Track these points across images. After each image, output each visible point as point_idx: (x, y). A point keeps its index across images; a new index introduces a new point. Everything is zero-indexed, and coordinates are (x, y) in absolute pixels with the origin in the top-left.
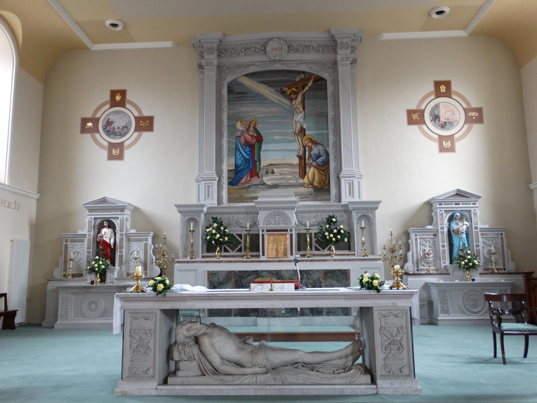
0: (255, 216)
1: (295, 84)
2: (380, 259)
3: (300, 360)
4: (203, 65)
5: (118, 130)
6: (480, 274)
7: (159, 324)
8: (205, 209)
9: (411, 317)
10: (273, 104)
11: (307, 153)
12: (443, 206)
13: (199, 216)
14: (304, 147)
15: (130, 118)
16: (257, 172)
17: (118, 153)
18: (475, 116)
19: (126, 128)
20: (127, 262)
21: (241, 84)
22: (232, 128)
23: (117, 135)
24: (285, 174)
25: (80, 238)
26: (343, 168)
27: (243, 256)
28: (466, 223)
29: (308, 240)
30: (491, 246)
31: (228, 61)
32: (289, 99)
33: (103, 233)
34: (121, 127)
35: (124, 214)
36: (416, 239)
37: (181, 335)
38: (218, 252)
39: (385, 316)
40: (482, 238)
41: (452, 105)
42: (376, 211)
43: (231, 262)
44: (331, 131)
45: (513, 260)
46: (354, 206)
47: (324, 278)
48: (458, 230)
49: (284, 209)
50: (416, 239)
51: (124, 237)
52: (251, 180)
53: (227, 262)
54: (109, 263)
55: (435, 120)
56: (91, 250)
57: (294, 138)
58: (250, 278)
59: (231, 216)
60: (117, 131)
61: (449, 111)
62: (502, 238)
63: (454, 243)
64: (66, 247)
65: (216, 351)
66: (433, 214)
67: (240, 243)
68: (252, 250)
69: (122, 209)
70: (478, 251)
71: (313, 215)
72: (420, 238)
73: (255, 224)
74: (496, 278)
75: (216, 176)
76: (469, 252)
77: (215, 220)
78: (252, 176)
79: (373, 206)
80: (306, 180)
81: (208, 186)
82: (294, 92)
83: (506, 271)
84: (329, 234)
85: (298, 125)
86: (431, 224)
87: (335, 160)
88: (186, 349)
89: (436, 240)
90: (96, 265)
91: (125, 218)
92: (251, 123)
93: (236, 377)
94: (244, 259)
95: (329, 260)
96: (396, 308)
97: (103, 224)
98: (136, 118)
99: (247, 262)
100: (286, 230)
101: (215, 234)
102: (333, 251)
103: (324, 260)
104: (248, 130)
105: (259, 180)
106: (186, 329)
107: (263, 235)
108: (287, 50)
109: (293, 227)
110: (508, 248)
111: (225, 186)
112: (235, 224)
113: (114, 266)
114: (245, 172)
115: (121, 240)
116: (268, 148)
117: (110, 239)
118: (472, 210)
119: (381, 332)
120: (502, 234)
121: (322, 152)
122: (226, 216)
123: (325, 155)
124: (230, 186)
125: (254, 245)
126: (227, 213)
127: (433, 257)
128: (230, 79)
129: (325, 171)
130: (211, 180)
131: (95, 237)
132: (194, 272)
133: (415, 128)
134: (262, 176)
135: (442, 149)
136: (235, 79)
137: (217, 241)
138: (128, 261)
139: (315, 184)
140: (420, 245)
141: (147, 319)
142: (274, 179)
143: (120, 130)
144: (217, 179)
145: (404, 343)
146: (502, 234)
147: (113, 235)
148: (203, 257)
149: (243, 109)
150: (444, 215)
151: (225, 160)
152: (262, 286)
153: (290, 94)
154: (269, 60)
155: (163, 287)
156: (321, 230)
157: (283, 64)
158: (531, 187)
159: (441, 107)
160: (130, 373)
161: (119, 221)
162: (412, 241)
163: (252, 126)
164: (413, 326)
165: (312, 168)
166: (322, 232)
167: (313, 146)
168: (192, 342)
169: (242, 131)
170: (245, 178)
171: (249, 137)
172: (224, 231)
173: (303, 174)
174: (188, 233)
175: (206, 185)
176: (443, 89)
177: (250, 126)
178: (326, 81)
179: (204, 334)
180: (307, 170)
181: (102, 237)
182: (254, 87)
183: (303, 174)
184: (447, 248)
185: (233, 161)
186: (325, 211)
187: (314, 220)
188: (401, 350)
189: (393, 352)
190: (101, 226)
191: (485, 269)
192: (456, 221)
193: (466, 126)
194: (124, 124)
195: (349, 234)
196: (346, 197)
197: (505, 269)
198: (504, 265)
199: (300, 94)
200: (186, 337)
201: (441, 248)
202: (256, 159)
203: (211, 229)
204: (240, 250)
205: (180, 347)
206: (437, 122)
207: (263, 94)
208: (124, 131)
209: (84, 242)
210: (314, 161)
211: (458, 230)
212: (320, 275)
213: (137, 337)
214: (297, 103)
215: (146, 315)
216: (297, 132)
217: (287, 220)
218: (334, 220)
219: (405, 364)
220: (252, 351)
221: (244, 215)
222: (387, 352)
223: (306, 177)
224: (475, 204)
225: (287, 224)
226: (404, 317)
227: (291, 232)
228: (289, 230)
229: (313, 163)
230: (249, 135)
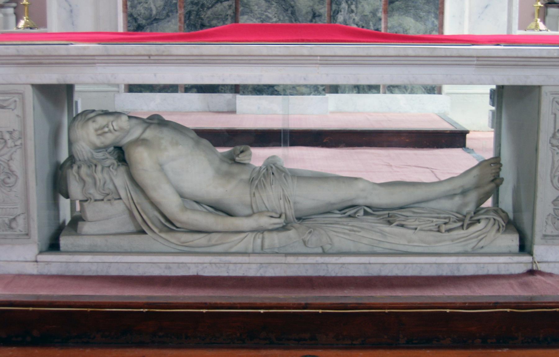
3: (360, 201)
65: (169, 181)
88: (99, 176)
93: (215, 237)
106: (96, 130)
168: (111, 160)
179: (140, 141)
200: (98, 149)
205: (84, 170)
220: (251, 181)
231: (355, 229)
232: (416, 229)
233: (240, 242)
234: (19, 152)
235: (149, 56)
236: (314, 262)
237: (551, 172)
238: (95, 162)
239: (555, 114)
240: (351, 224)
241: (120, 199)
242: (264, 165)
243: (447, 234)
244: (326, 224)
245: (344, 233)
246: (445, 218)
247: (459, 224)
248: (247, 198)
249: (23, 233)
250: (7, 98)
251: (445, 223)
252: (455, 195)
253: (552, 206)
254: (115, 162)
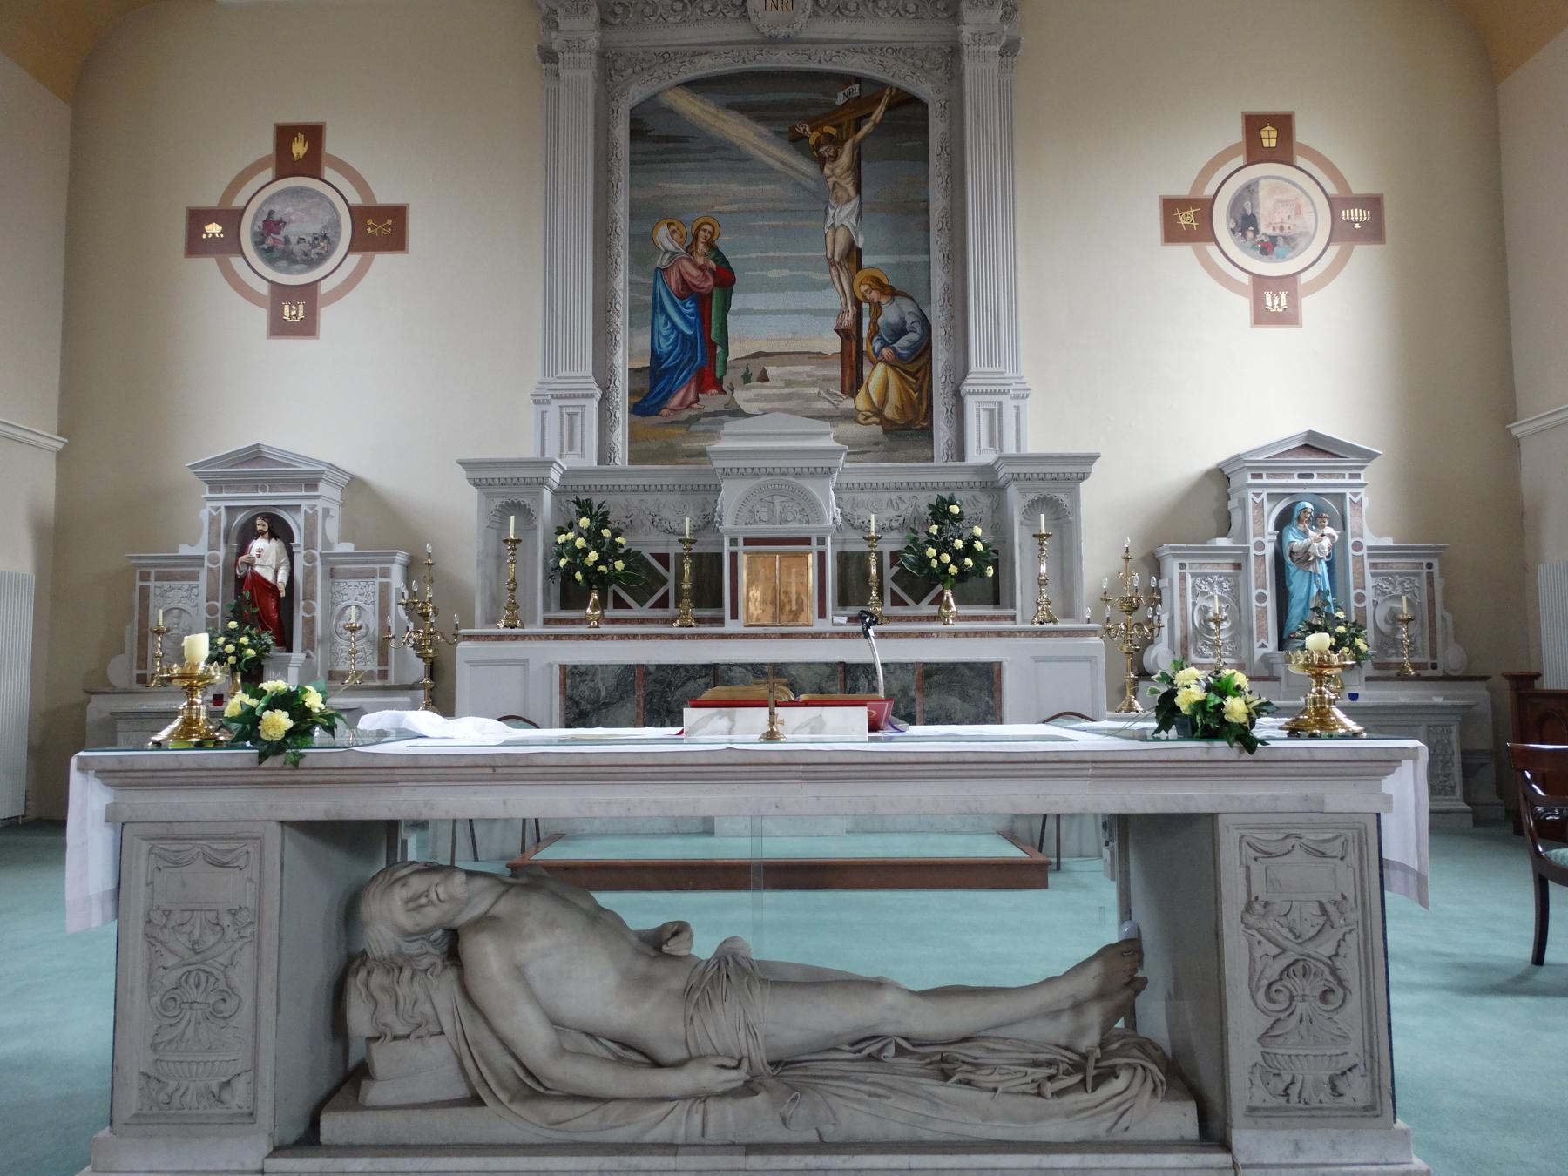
0: (710, 497)
2: (1093, 632)
3: (888, 1029)
4: (555, 48)
5: (302, 246)
6: (1368, 679)
8: (555, 476)
9: (1381, 859)
11: (866, 321)
12: (1265, 481)
13: (538, 497)
14: (858, 304)
15: (336, 211)
16: (718, 375)
17: (301, 316)
19: (323, 242)
20: (329, 639)
21: (670, 111)
22: (642, 245)
23: (296, 262)
24: (799, 383)
26: (973, 367)
27: (673, 620)
28: (1328, 530)
29: (874, 571)
30: (1399, 598)
32: (813, 159)
33: (254, 553)
34: (309, 239)
35: (317, 497)
36: (1183, 578)
37: (382, 928)
38: (595, 607)
39: (1269, 855)
40: (1374, 575)
41: (1295, 185)
42: (1083, 485)
43: (634, 637)
44: (937, 255)
45: (1457, 639)
46: (1016, 470)
47: (920, 689)
48: (1306, 551)
49: (798, 474)
50: (1183, 578)
51: (318, 563)
52: (697, 400)
53: (622, 637)
54: (270, 641)
55: (1243, 231)
56: (219, 605)
57: (827, 277)
58: (691, 686)
59: (634, 498)
60: (296, 248)
61: (1285, 203)
62: (1430, 577)
63: (1291, 588)
64: (144, 592)
65: (534, 998)
66: (1232, 504)
67: (664, 581)
68: (698, 604)
69: (310, 481)
70: (1361, 612)
71: (886, 496)
72: (1193, 575)
73: (708, 523)
74: (1418, 692)
75: (595, 386)
76: (1341, 615)
77: (585, 508)
78: (701, 389)
79: (1076, 468)
80: (861, 402)
81: (571, 415)
82: (830, 139)
83: (1438, 673)
84: (939, 554)
85: (841, 237)
86: (1224, 533)
87: (947, 342)
88: (403, 990)
89: (1241, 580)
90: (230, 648)
91: (319, 509)
92: (699, 228)
93: (615, 1110)
94: (675, 629)
95: (938, 634)
96: (1316, 818)
97: (255, 525)
98: (352, 210)
99: (682, 637)
100: (807, 541)
101: (585, 552)
102: (948, 606)
103: (922, 634)
104: (691, 249)
105: (724, 399)
106: (407, 902)
107: (734, 556)
108: (809, 6)
109: (828, 530)
110: (1446, 606)
111: (622, 415)
112: (649, 524)
113: (290, 650)
114: (682, 374)
115: (309, 574)
116: (748, 306)
117: (276, 572)
118: (1348, 492)
119: (1251, 920)
120: (1430, 566)
121: (909, 320)
122: (620, 498)
123: (918, 327)
124: (637, 418)
125: (707, 589)
126: (623, 490)
127: (1230, 628)
128: (637, 92)
129: (920, 375)
130: (578, 397)
131: (230, 567)
132: (517, 670)
133: (1185, 251)
134: (732, 390)
135: (1262, 317)
136: (654, 96)
137: (590, 572)
138: (331, 636)
139: (889, 412)
140: (1192, 593)
141: (223, 865)
142: (766, 398)
143: (305, 247)
144: (598, 394)
145: (1350, 968)
146: (1430, 566)
147: (285, 559)
148: (547, 622)
149: (677, 187)
150: (1267, 507)
151: (622, 337)
152: (732, 720)
153: (818, 145)
154: (757, 37)
155: (289, 724)
156: (914, 541)
157: (797, 52)
158: (1515, 432)
159: (1262, 193)
160: (147, 1095)
161: (301, 519)
162: (1171, 581)
164: (1387, 894)
165: (881, 366)
166: (915, 547)
167: (883, 300)
168: (432, 956)
169: (673, 254)
170: (681, 394)
171: (695, 272)
172: (612, 542)
173: (853, 383)
175: (565, 411)
176: (1269, 138)
177: (696, 238)
178: (925, 106)
179: (485, 922)
180: (866, 371)
181: (251, 564)
182: (708, 118)
183: (853, 383)
184: (1270, 604)
185: (644, 342)
186: (923, 487)
187: (892, 513)
188: (1335, 1000)
189: (1301, 1007)
190: (247, 534)
191: (1377, 666)
192: (1301, 527)
193: (1334, 250)
194: (316, 228)
195: (998, 555)
196: (980, 451)
197: (1434, 667)
198: (1434, 656)
199: (848, 146)
200: (409, 936)
201: (1254, 603)
202: (713, 337)
203: (571, 535)
204: (663, 603)
205: (378, 978)
206: (1250, 235)
207: (739, 142)
208: (317, 250)
209: (197, 579)
210: (885, 345)
211: (1306, 551)
212: (911, 679)
213: (180, 943)
214: (838, 171)
215: (222, 849)
216: (837, 259)
217: (810, 509)
218: (955, 509)
219: (1351, 1060)
220: (688, 992)
221: (677, 497)
222: (1277, 1007)
223: (862, 392)
224: (1358, 476)
225: (808, 522)
226: (1352, 858)
227: (821, 548)
228: (814, 541)
229: (885, 351)
230: (695, 264)
231: (880, 1091)
232: (995, 1090)
233: (658, 1123)
234: (248, 950)
235: (494, 767)
236: (801, 1166)
237: (1251, 979)
238: (400, 961)
239: (1248, 868)
240: (872, 1078)
241: (442, 1033)
242: (715, 956)
243: (1055, 1101)
244: (826, 1077)
245: (859, 1101)
246: (1050, 1064)
247: (1077, 1078)
248: (680, 1029)
249: (245, 1110)
250: (233, 846)
251: (1051, 1078)
252: (1061, 1011)
253: (1259, 1049)
254: (439, 962)
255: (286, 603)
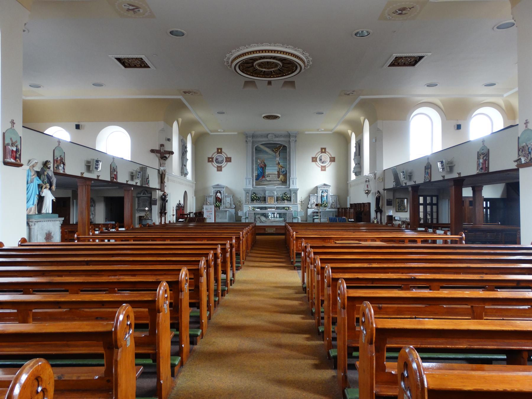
1: (277, 148)
7: (253, 215)
10: (270, 154)
18: (333, 160)
19: (222, 161)
22: (256, 162)
25: (211, 196)
31: (255, 140)
73: (265, 194)
77: (254, 193)
79: (297, 189)
111: (254, 180)
114: (261, 176)
125: (264, 200)
128: (256, 146)
135: (322, 170)
163: (263, 162)
173: (279, 177)
174: (246, 197)
176: (323, 150)
183: (279, 177)
195: (290, 197)
215: (252, 214)
217: (274, 193)
255: (221, 200)
